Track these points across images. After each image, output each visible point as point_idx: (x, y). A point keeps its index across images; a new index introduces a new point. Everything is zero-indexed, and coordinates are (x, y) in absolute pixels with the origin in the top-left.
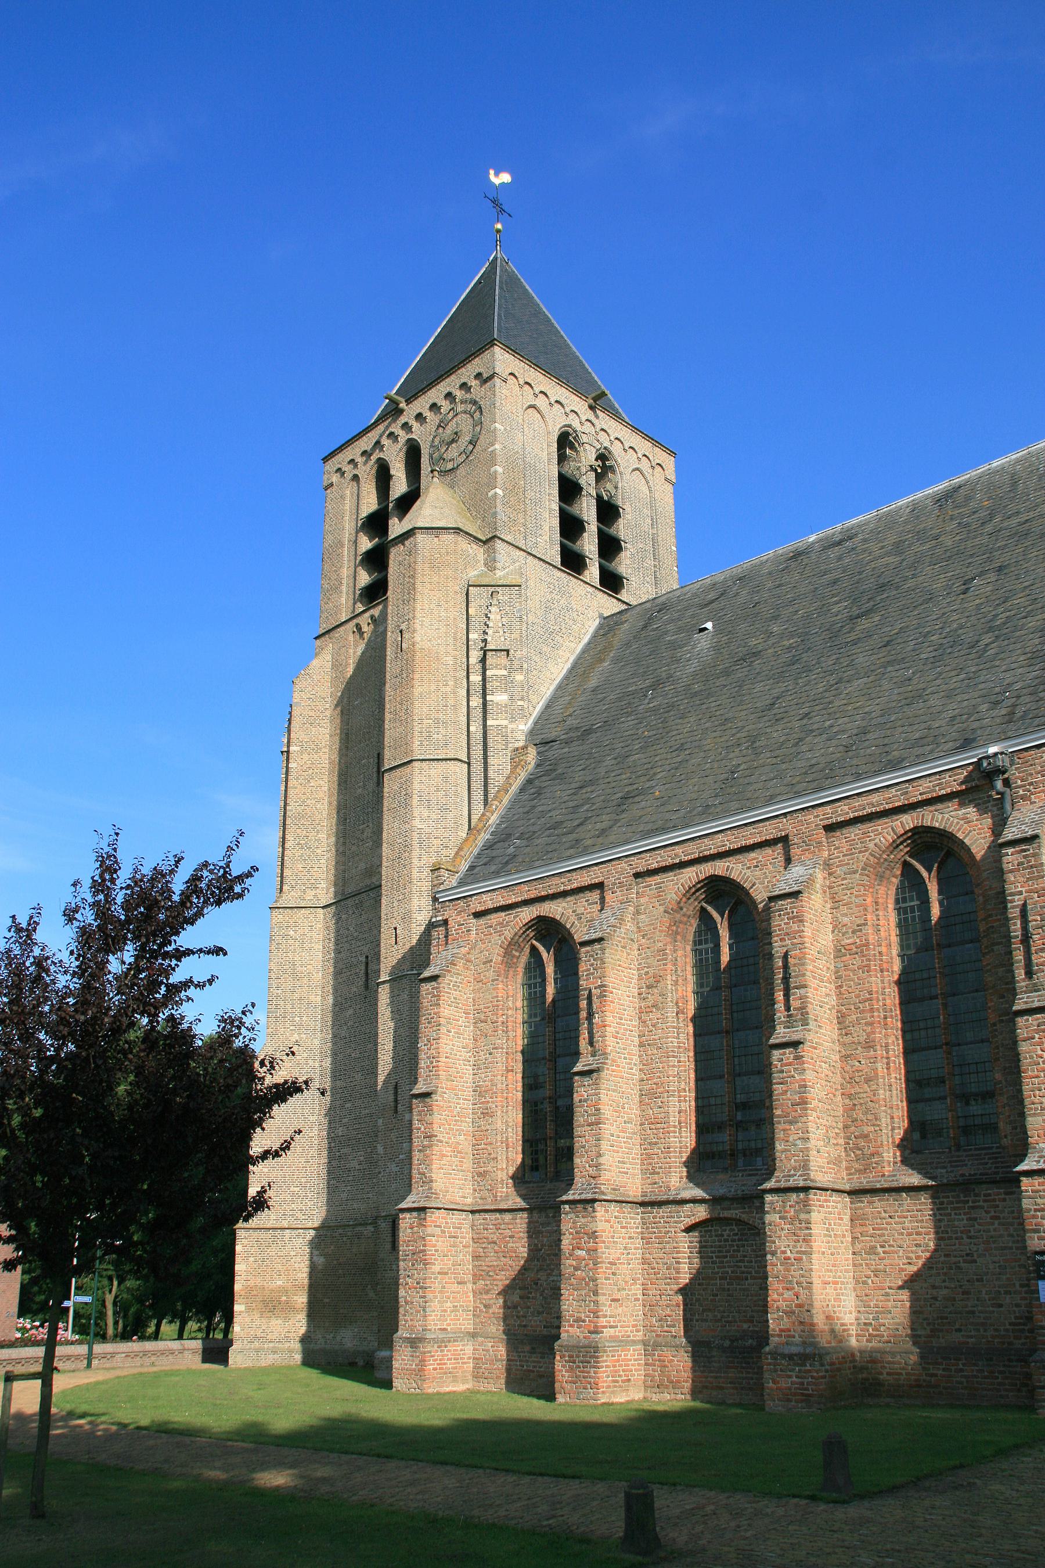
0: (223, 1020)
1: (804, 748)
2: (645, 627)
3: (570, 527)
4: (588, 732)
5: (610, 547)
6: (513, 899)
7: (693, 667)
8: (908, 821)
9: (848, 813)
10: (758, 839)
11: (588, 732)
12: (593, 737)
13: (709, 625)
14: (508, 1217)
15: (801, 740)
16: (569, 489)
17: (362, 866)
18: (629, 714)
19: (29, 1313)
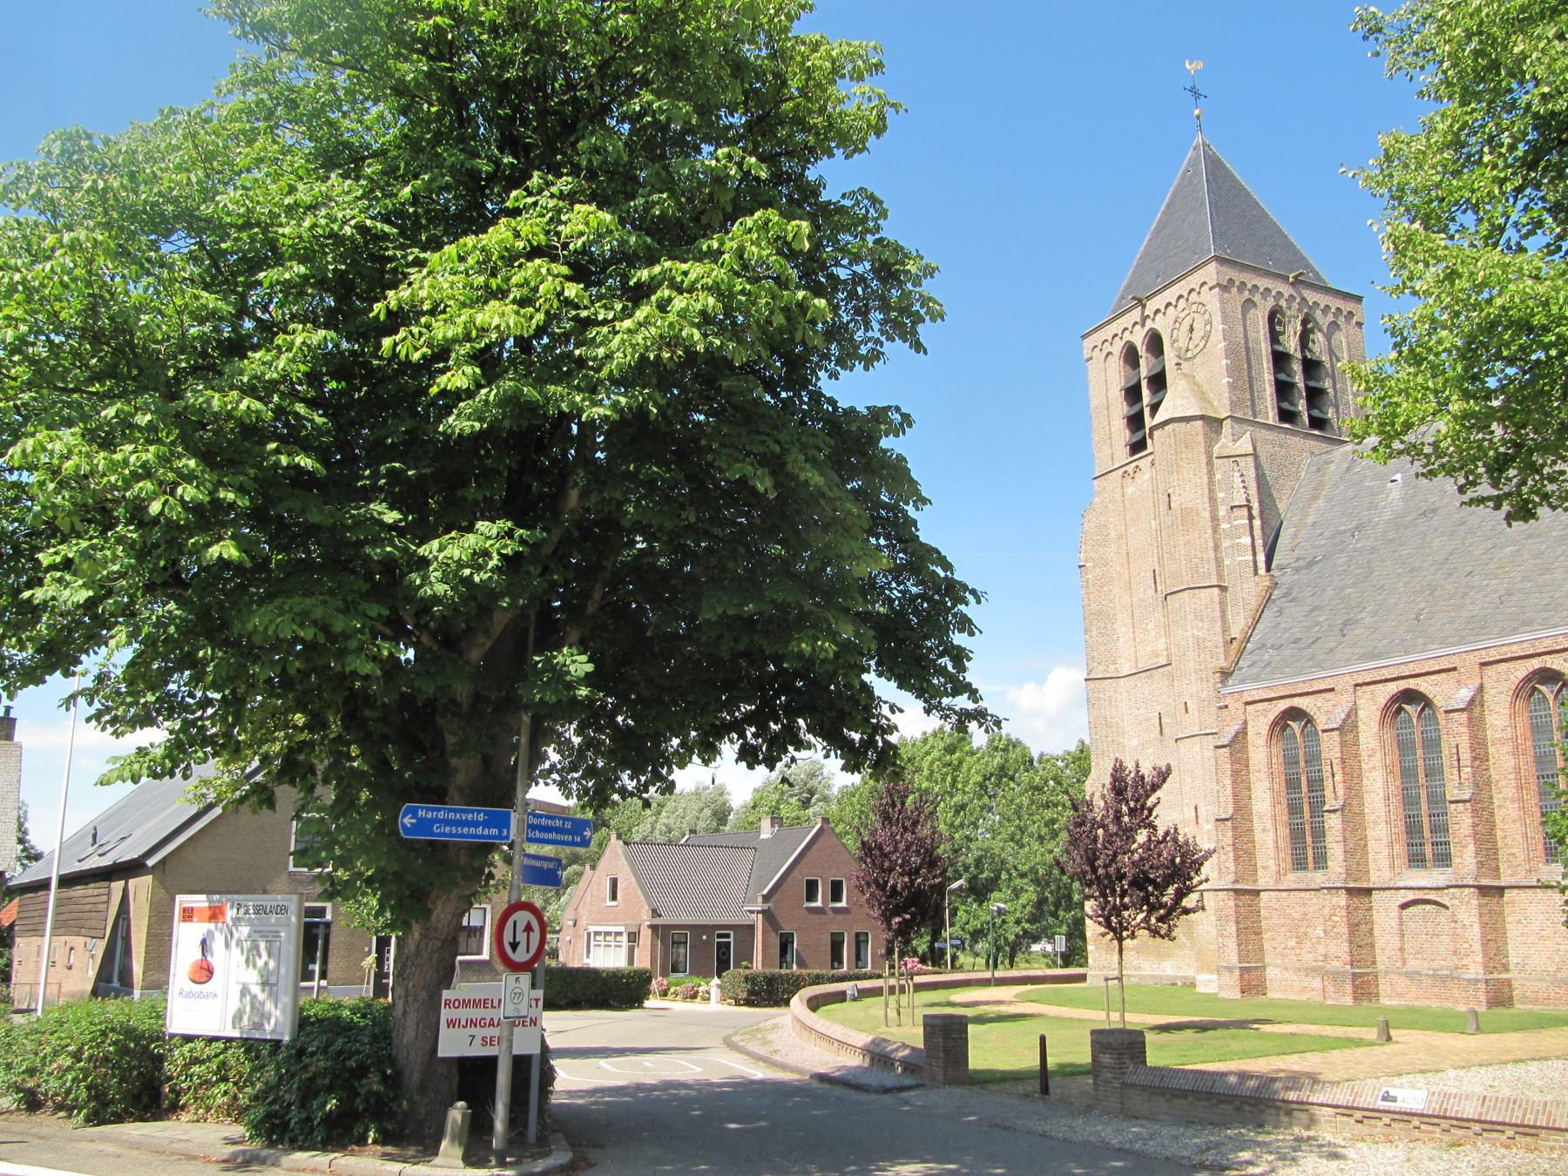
0: (1168, 936)
1: (1467, 600)
2: (1348, 469)
3: (1283, 389)
4: (1312, 563)
5: (1315, 395)
6: (1273, 695)
7: (1388, 515)
8: (1536, 664)
9: (1457, 1001)
10: (1437, 668)
11: (1312, 563)
12: (1316, 568)
13: (1398, 477)
14: (1284, 894)
15: (1466, 594)
16: (1280, 360)
17: (1149, 649)
18: (1342, 551)
19: (736, 688)
